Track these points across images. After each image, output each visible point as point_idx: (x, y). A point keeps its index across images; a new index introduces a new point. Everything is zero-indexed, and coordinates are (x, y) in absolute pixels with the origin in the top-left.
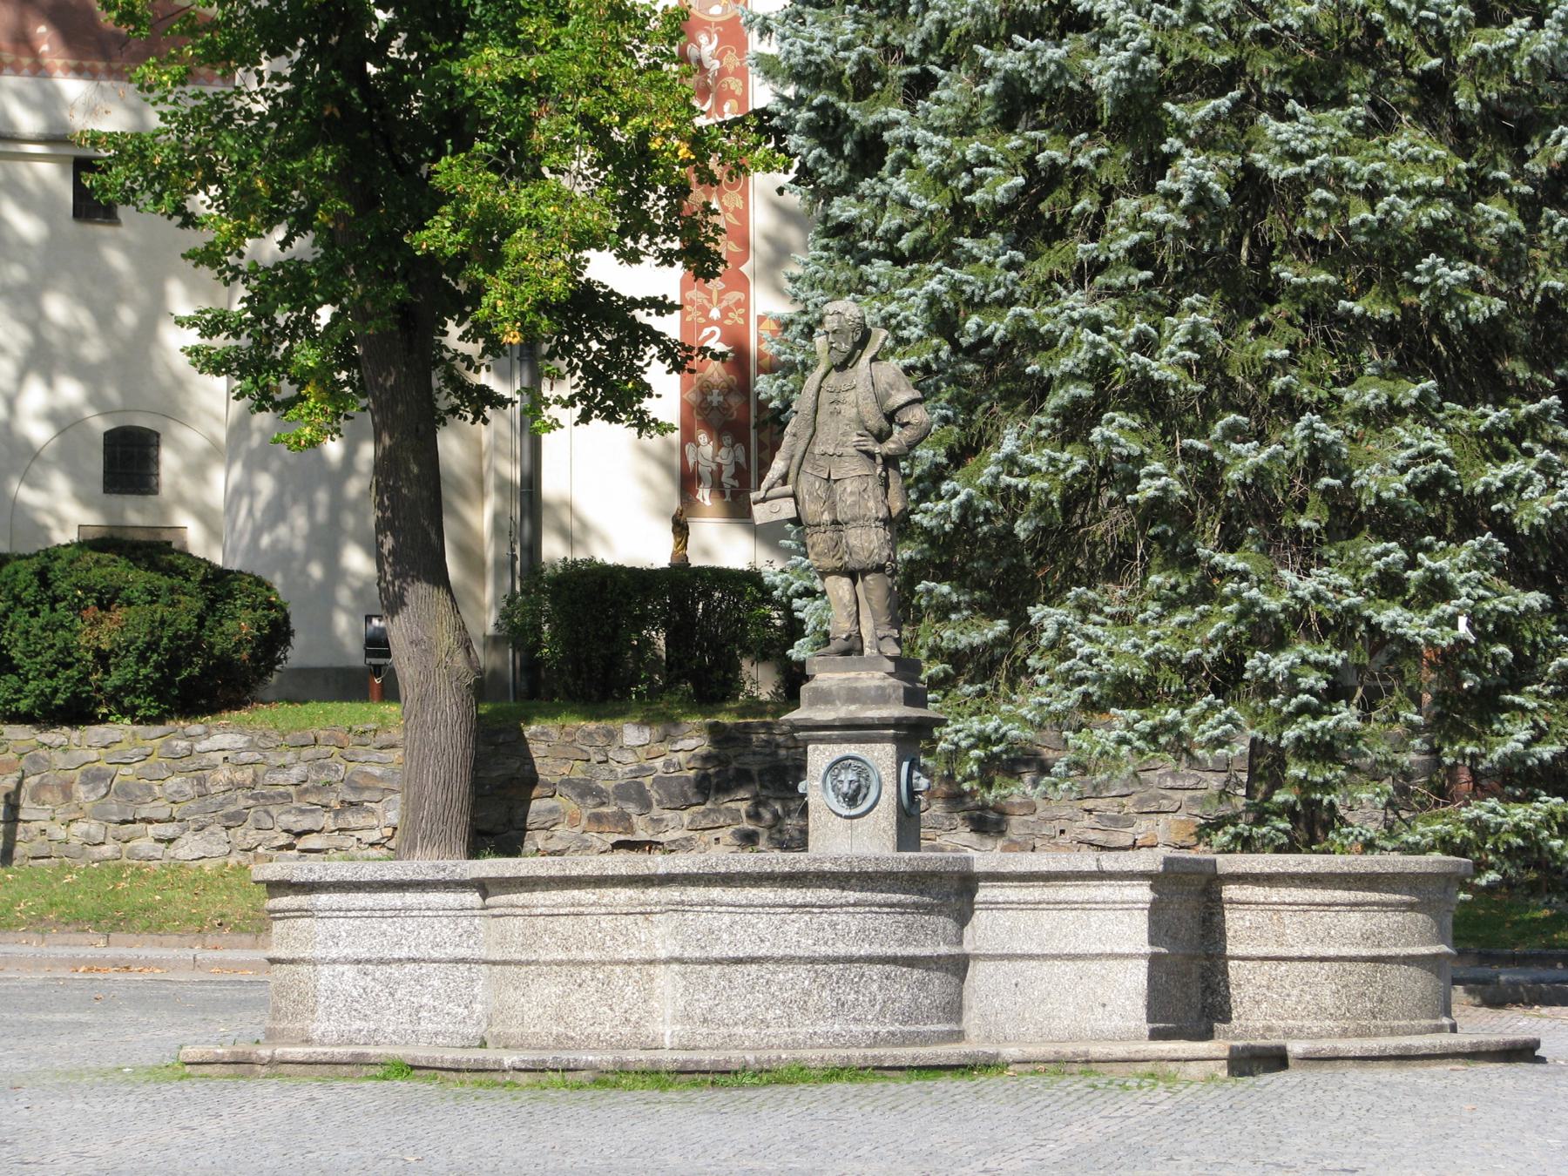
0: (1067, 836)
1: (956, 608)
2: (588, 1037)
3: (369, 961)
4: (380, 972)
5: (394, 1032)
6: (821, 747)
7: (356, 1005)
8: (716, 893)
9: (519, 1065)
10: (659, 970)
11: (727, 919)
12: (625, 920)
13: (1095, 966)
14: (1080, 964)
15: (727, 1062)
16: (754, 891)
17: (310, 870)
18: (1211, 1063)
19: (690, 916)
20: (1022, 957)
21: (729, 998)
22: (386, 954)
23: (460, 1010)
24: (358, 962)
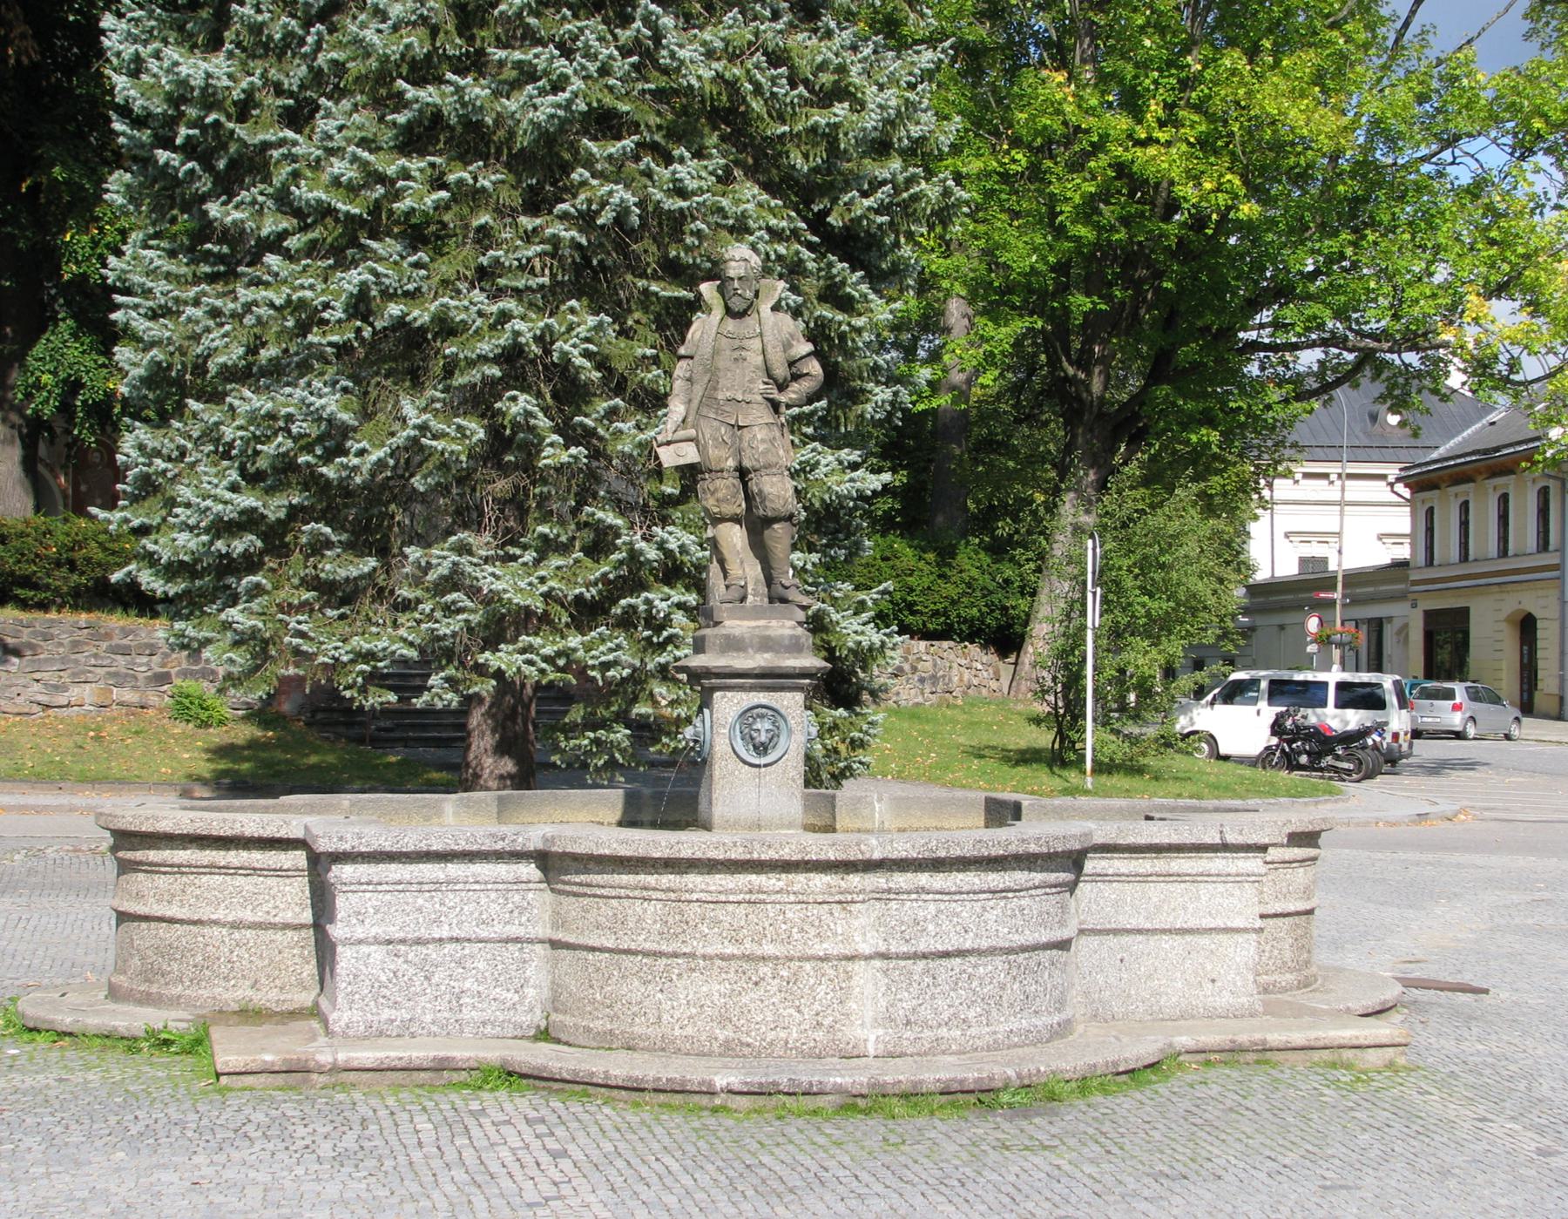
0: (22, 698)
1: (329, 544)
2: (771, 1044)
3: (403, 941)
4: (413, 953)
5: (433, 1022)
6: (729, 694)
7: (384, 991)
8: (924, 879)
9: (737, 1087)
10: (858, 966)
11: (932, 907)
12: (815, 910)
13: (1204, 941)
14: (1188, 938)
15: (991, 1079)
16: (961, 876)
17: (341, 839)
18: (1390, 1050)
19: (893, 905)
20: (1129, 931)
21: (933, 997)
22: (424, 933)
23: (509, 995)
24: (389, 942)
